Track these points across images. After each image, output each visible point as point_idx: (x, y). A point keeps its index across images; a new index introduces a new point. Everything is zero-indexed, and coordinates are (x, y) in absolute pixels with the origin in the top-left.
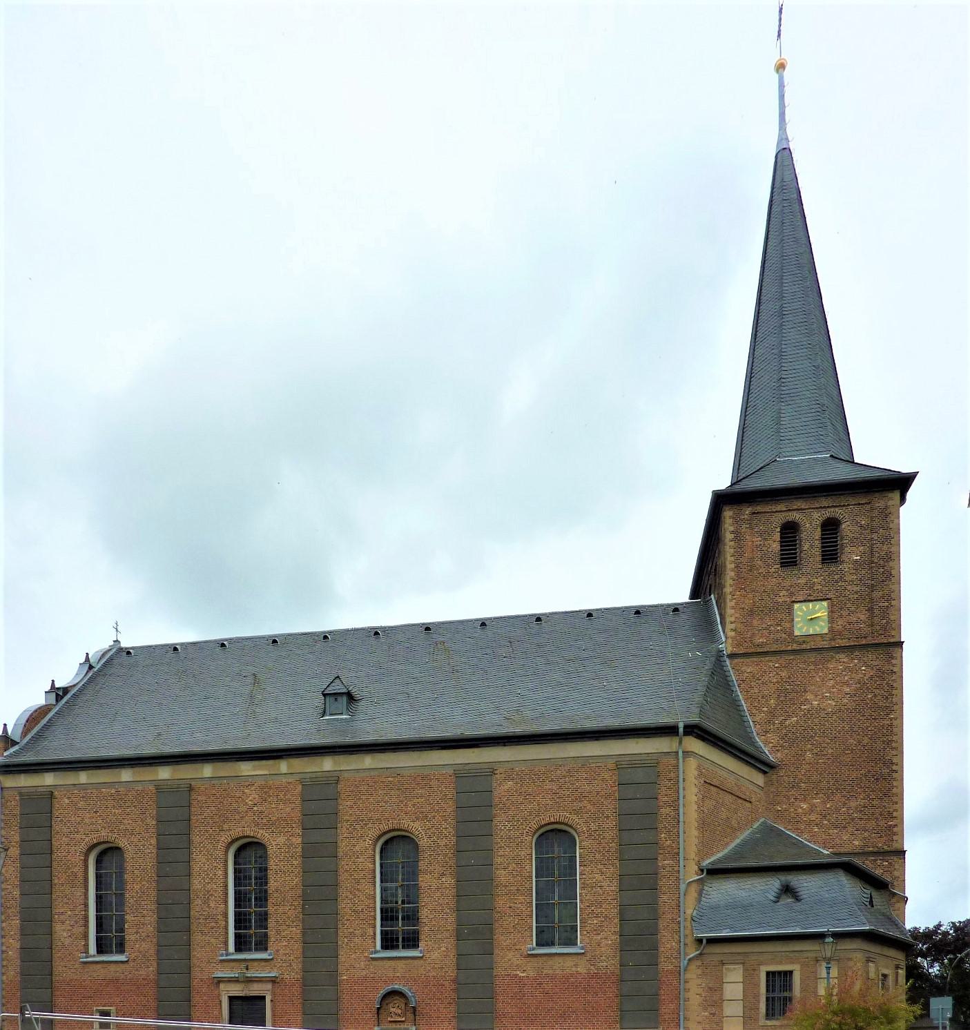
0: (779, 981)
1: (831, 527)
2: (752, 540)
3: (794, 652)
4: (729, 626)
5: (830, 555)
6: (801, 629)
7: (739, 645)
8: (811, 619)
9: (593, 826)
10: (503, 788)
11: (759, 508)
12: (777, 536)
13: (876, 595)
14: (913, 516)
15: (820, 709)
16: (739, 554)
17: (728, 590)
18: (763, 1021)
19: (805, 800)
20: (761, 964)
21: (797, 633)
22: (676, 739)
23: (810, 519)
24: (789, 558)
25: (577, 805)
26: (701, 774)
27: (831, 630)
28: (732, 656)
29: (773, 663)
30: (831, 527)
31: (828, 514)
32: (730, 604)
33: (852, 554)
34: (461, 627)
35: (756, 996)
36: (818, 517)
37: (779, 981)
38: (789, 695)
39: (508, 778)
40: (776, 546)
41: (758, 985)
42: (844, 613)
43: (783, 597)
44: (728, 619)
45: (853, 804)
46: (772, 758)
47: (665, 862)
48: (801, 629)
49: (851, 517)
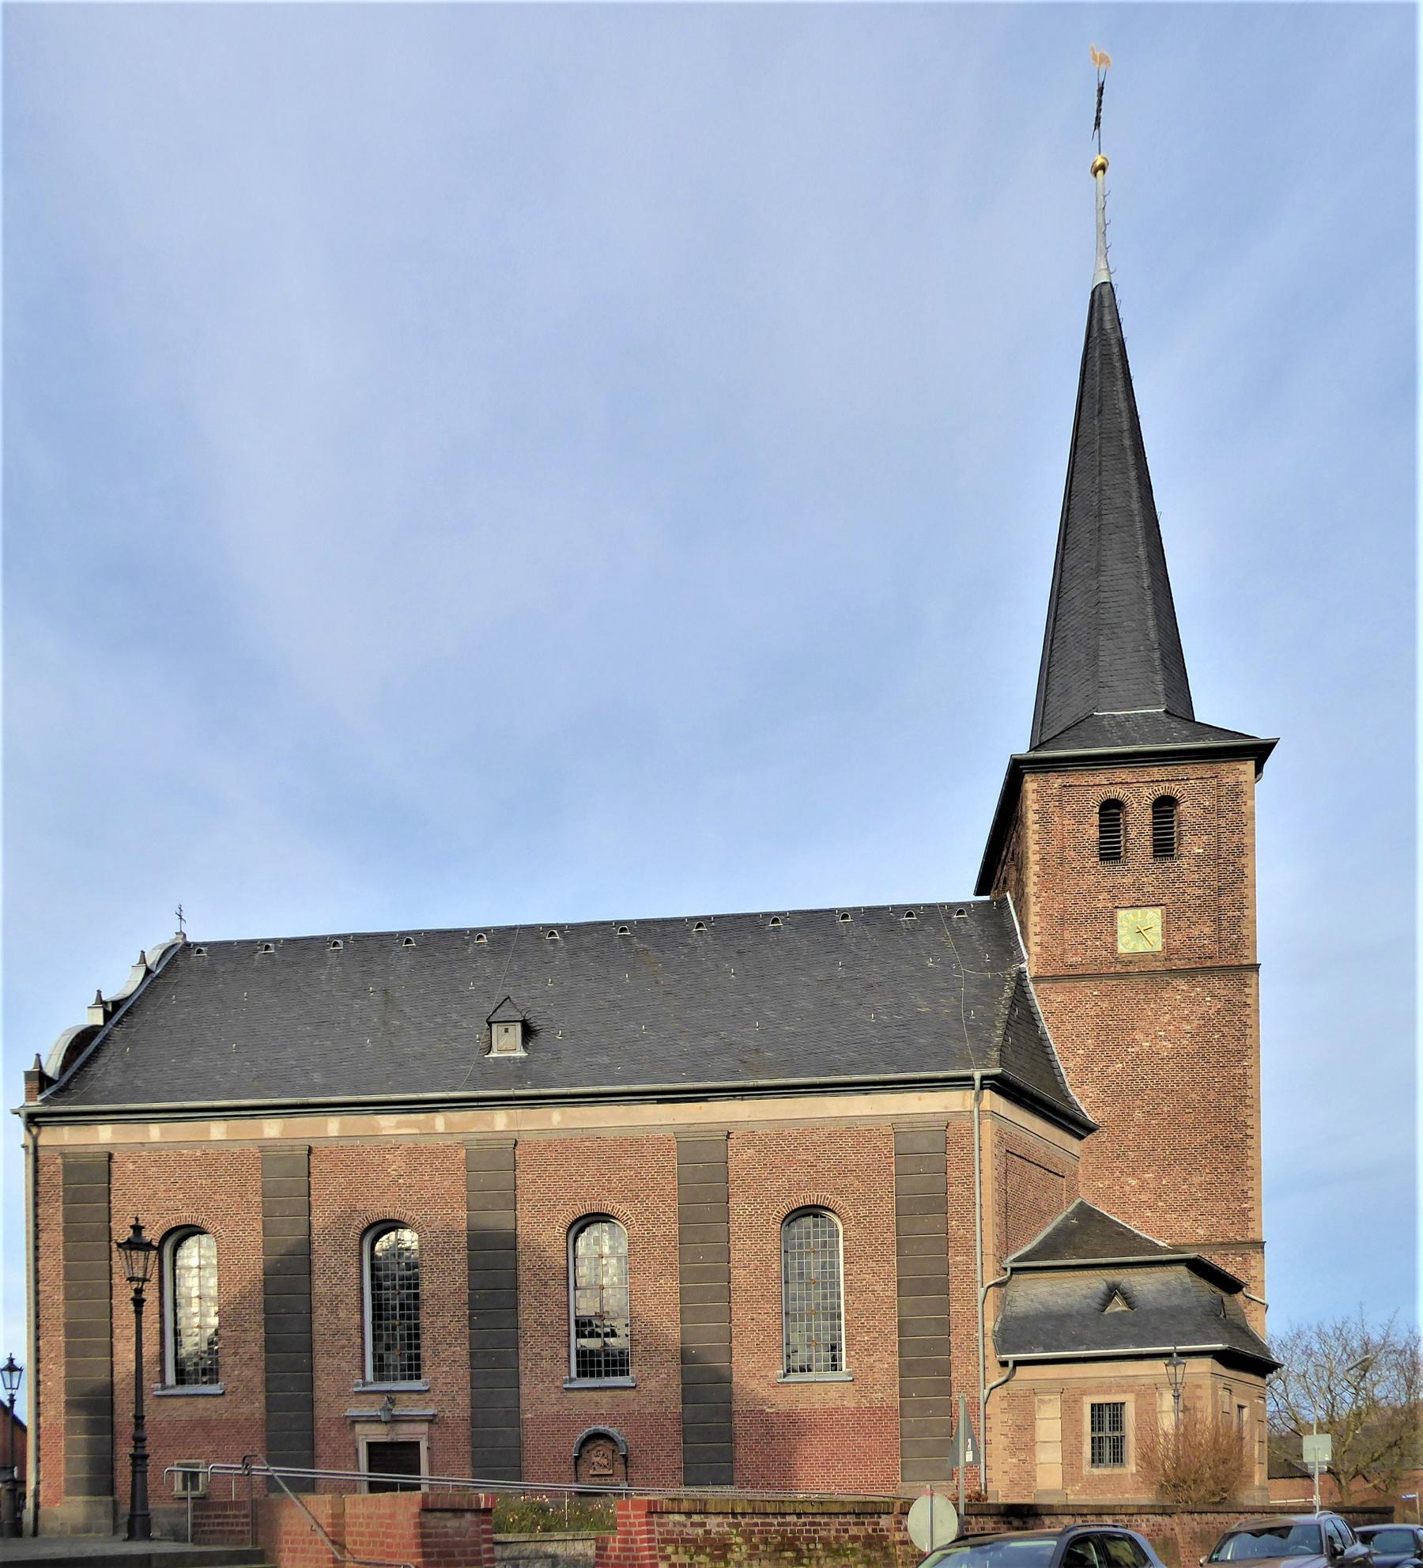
0: (1107, 1416)
1: (1164, 806)
2: (1062, 823)
3: (1118, 975)
4: (1033, 939)
5: (1164, 847)
7: (1046, 964)
9: (863, 1211)
10: (740, 1159)
11: (1071, 780)
13: (1226, 900)
14: (1269, 795)
15: (1152, 1053)
17: (1031, 889)
18: (1087, 1469)
19: (1133, 1174)
23: (1138, 791)
24: (1110, 851)
28: (1037, 979)
30: (1164, 806)
31: (1162, 790)
33: (1192, 846)
35: (1079, 1436)
36: (1149, 794)
37: (1107, 1416)
39: (749, 1144)
40: (1094, 833)
43: (1102, 901)
45: (1196, 1180)
47: (956, 1259)
48: (1127, 944)
49: (1191, 787)
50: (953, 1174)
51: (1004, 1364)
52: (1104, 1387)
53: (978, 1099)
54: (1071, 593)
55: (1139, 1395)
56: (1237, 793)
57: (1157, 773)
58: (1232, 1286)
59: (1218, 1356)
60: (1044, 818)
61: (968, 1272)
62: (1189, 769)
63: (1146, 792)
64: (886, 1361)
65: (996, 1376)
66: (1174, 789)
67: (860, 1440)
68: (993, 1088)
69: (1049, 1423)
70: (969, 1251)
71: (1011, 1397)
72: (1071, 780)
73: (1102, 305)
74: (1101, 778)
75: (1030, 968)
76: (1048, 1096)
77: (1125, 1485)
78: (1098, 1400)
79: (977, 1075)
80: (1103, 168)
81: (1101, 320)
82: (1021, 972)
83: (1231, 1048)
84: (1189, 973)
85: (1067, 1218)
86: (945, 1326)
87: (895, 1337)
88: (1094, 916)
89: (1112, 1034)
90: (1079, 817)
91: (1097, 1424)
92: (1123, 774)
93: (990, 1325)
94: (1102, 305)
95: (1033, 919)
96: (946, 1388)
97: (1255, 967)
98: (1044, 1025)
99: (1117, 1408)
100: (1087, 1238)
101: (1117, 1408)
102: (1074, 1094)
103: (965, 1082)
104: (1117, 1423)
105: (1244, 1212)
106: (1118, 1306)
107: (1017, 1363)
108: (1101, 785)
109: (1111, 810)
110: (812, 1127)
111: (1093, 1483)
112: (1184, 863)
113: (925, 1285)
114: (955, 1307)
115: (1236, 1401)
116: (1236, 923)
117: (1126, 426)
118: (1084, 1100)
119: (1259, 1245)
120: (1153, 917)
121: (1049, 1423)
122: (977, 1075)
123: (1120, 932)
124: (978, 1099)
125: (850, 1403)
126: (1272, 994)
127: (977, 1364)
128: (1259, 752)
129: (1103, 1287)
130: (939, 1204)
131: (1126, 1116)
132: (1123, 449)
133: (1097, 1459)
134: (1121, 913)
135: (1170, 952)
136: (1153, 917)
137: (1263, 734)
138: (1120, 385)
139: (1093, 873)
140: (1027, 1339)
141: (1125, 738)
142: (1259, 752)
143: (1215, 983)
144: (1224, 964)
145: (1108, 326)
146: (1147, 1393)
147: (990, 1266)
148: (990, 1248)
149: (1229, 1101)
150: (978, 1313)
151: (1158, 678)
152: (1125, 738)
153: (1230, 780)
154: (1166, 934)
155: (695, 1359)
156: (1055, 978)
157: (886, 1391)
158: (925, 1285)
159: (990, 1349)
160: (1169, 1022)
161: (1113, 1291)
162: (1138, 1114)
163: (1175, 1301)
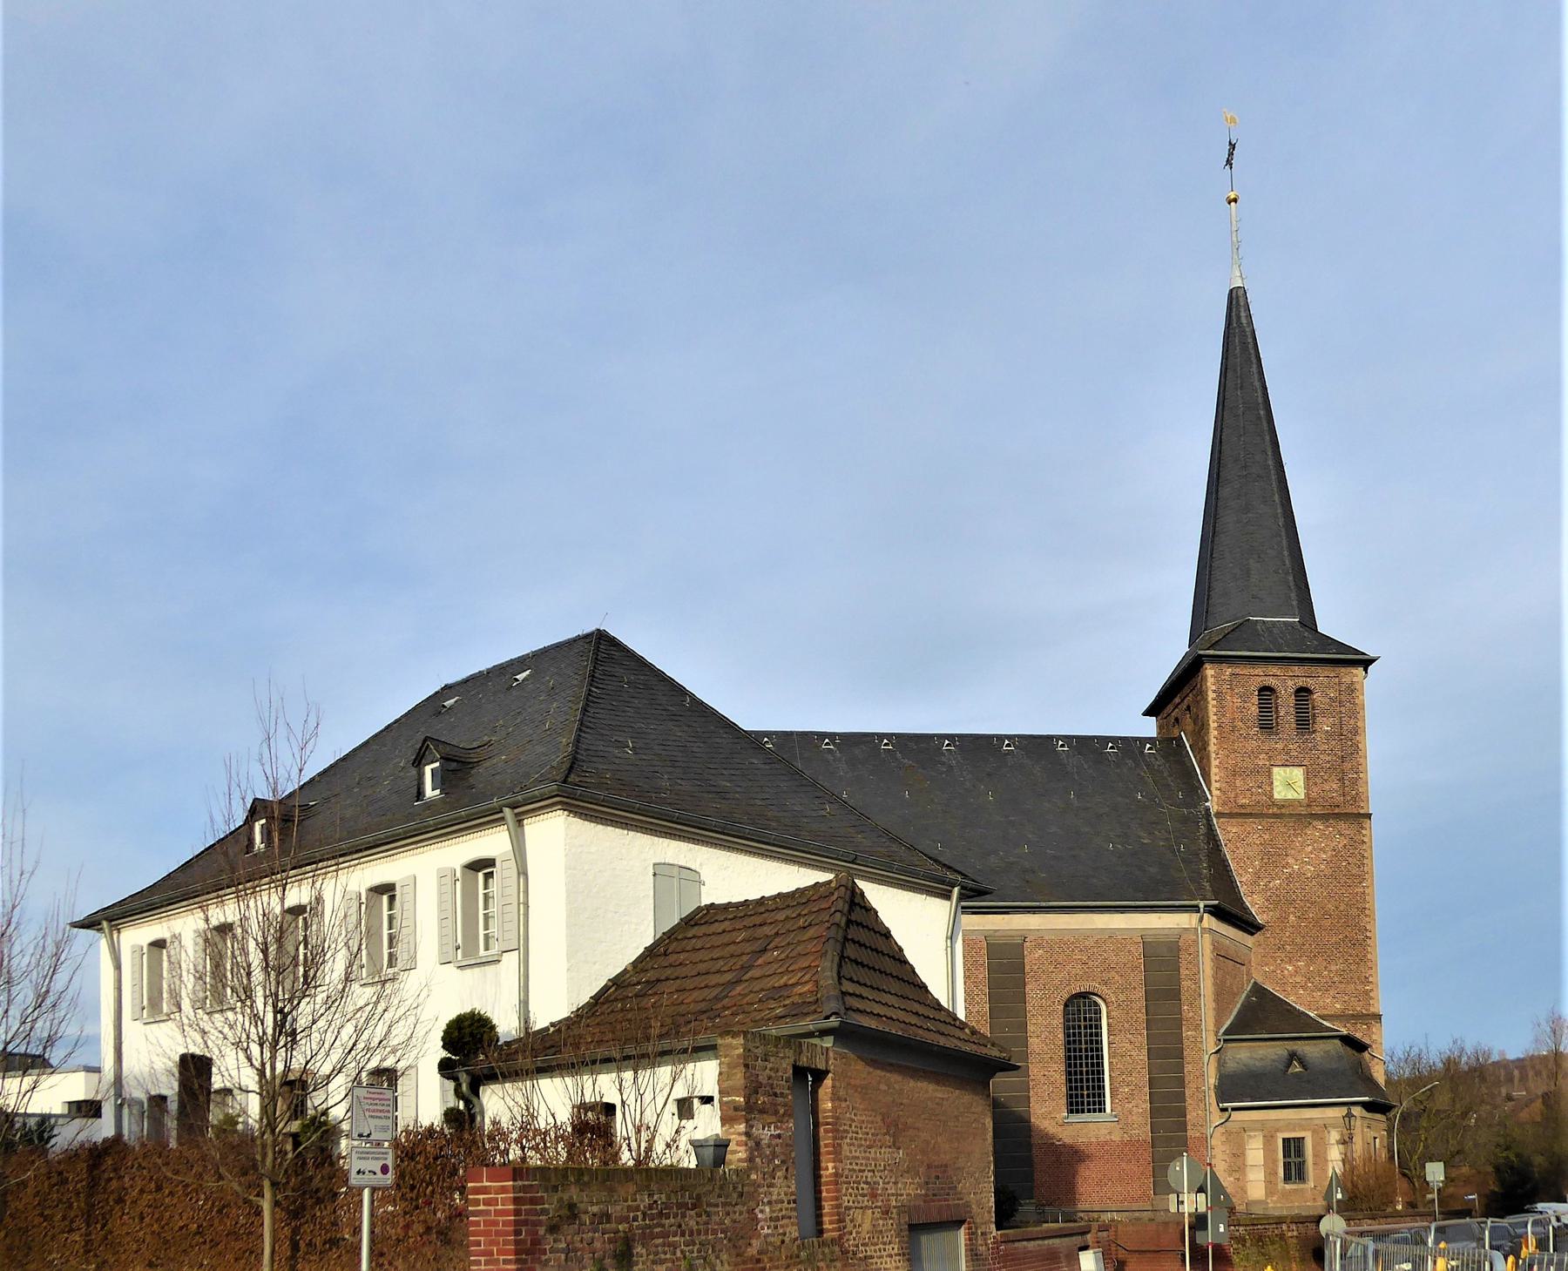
0: (1293, 1148)
1: (1303, 692)
2: (1233, 701)
3: (1275, 816)
4: (1215, 785)
5: (1304, 722)
6: (1280, 793)
7: (1224, 804)
8: (1288, 784)
9: (1122, 997)
10: (1032, 957)
11: (1237, 671)
12: (1255, 700)
13: (1347, 765)
14: (1371, 684)
15: (1301, 874)
16: (1221, 706)
17: (1212, 748)
18: (1281, 1185)
19: (1290, 962)
20: (1278, 1130)
21: (1276, 796)
22: (1196, 916)
23: (1285, 681)
24: (1267, 725)
25: (1105, 976)
26: (1215, 948)
27: (1307, 795)
28: (1219, 815)
29: (1254, 825)
30: (1303, 692)
31: (1301, 683)
32: (1214, 763)
33: (1324, 725)
34: (912, 745)
35: (1275, 1161)
36: (1291, 685)
37: (1293, 1148)
38: (1272, 857)
39: (1039, 946)
40: (1254, 710)
41: (1275, 1151)
42: (1319, 781)
43: (1262, 760)
44: (1213, 778)
45: (1333, 968)
46: (1260, 919)
47: (1187, 1033)
48: (1280, 793)
49: (1321, 681)
50: (1183, 972)
51: (1224, 1110)
52: (1291, 1125)
53: (1201, 920)
54: (1228, 519)
55: (1314, 1132)
56: (1352, 690)
57: (1297, 670)
58: (1360, 1047)
59: (1365, 1105)
60: (1220, 695)
61: (1197, 1041)
62: (1319, 670)
63: (1290, 683)
64: (1141, 1105)
65: (1217, 1117)
66: (1310, 683)
67: (1124, 1165)
68: (1210, 913)
69: (1255, 1153)
70: (1197, 1027)
71: (1228, 1133)
72: (1237, 671)
73: (1237, 303)
74: (1259, 671)
75: (1213, 805)
76: (1235, 910)
77: (1306, 1197)
78: (1287, 1135)
79: (1201, 905)
80: (1235, 200)
81: (1239, 317)
82: (1208, 809)
83: (1351, 872)
84: (1324, 817)
85: (1248, 997)
86: (1181, 1082)
87: (1147, 1089)
88: (1257, 771)
89: (1272, 857)
90: (1244, 697)
91: (1286, 1154)
92: (1274, 670)
93: (1212, 1080)
94: (1237, 303)
95: (1214, 770)
96: (1183, 1127)
97: (1369, 816)
98: (1225, 850)
99: (1300, 1140)
100: (1261, 1014)
101: (1300, 1140)
102: (1247, 901)
103: (1195, 909)
104: (1300, 1152)
105: (1367, 993)
106: (1297, 1068)
107: (1234, 1109)
108: (1260, 675)
109: (1266, 691)
110: (1087, 934)
111: (1285, 1194)
112: (1318, 736)
113: (1167, 1052)
114: (1188, 1068)
115: (1373, 1134)
116: (1355, 782)
117: (1260, 400)
118: (1255, 904)
119: (1378, 1017)
120: (1298, 774)
121: (1255, 1153)
122: (1201, 905)
123: (1276, 783)
124: (1201, 920)
125: (1116, 1137)
126: (1377, 829)
127: (1205, 1112)
128: (1366, 663)
129: (1286, 1053)
130: (1174, 995)
131: (1283, 919)
132: (1259, 418)
133: (1287, 1178)
134: (1275, 770)
135: (1310, 801)
136: (1298, 774)
137: (1372, 655)
138: (1254, 369)
139: (1254, 740)
140: (1237, 1088)
141: (1253, 593)
142: (1366, 663)
143: (1342, 825)
144: (1343, 810)
145: (1244, 321)
146: (1321, 1129)
147: (1212, 1039)
148: (1211, 1027)
149: (1354, 912)
150: (1203, 1071)
151: (1293, 595)
152: (1253, 593)
153: (1346, 680)
154: (1307, 787)
155: (1003, 1106)
156: (1231, 815)
157: (1142, 1130)
158: (1167, 1052)
159: (1213, 1100)
160: (1311, 852)
161: (1293, 1056)
162: (1292, 918)
163: (1334, 1066)
